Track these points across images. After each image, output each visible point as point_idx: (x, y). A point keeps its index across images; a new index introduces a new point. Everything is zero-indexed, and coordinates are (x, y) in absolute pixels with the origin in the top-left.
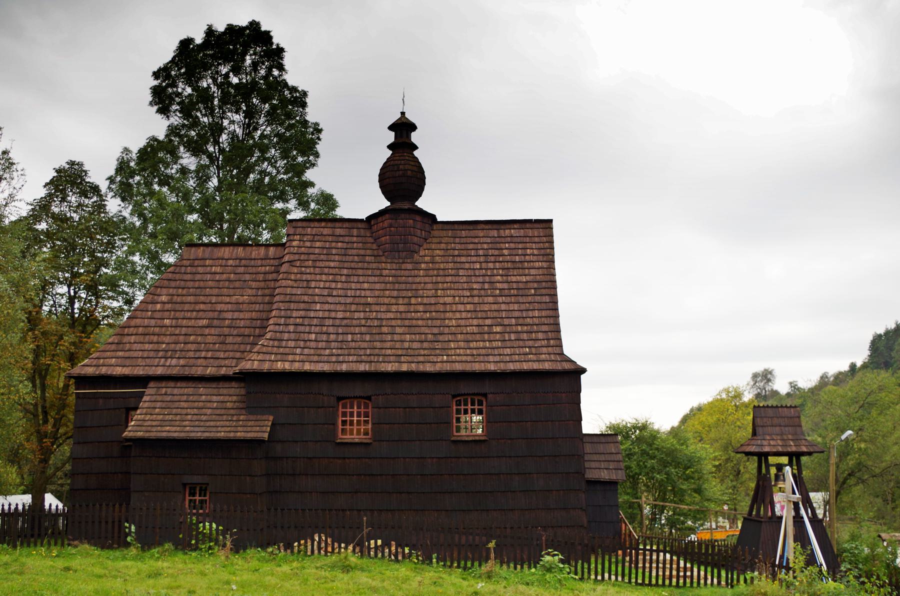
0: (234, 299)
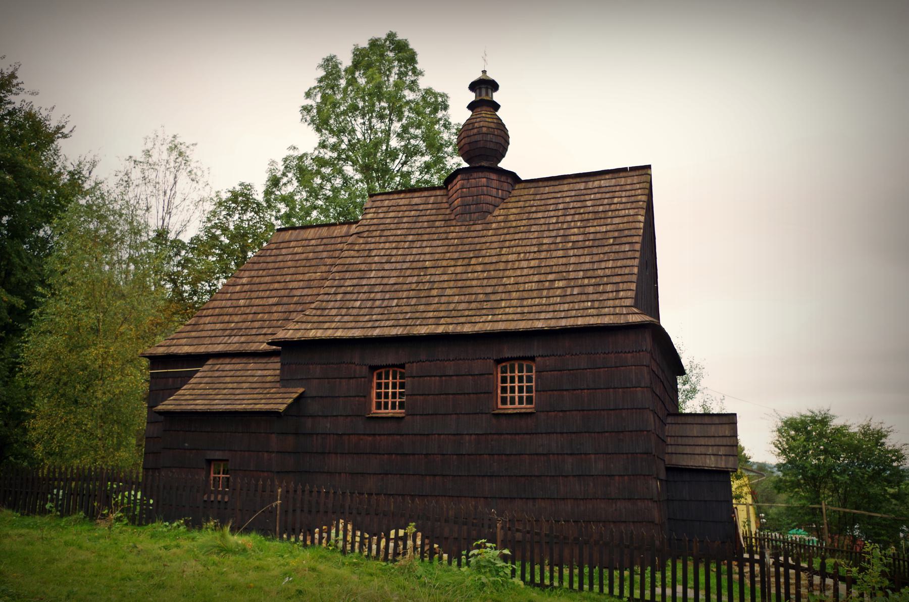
0: (307, 277)
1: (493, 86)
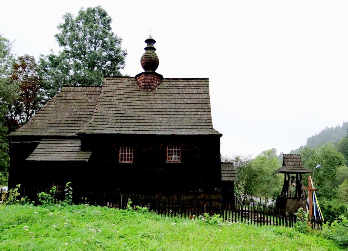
1: (153, 41)
